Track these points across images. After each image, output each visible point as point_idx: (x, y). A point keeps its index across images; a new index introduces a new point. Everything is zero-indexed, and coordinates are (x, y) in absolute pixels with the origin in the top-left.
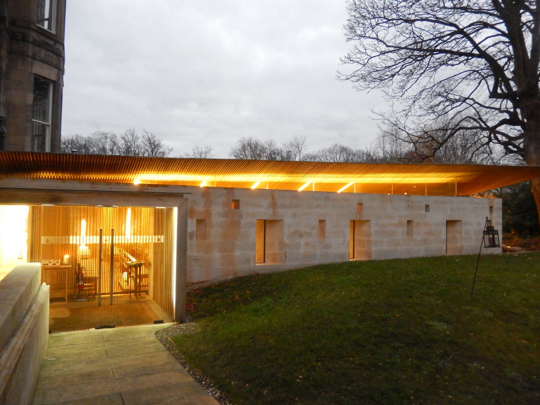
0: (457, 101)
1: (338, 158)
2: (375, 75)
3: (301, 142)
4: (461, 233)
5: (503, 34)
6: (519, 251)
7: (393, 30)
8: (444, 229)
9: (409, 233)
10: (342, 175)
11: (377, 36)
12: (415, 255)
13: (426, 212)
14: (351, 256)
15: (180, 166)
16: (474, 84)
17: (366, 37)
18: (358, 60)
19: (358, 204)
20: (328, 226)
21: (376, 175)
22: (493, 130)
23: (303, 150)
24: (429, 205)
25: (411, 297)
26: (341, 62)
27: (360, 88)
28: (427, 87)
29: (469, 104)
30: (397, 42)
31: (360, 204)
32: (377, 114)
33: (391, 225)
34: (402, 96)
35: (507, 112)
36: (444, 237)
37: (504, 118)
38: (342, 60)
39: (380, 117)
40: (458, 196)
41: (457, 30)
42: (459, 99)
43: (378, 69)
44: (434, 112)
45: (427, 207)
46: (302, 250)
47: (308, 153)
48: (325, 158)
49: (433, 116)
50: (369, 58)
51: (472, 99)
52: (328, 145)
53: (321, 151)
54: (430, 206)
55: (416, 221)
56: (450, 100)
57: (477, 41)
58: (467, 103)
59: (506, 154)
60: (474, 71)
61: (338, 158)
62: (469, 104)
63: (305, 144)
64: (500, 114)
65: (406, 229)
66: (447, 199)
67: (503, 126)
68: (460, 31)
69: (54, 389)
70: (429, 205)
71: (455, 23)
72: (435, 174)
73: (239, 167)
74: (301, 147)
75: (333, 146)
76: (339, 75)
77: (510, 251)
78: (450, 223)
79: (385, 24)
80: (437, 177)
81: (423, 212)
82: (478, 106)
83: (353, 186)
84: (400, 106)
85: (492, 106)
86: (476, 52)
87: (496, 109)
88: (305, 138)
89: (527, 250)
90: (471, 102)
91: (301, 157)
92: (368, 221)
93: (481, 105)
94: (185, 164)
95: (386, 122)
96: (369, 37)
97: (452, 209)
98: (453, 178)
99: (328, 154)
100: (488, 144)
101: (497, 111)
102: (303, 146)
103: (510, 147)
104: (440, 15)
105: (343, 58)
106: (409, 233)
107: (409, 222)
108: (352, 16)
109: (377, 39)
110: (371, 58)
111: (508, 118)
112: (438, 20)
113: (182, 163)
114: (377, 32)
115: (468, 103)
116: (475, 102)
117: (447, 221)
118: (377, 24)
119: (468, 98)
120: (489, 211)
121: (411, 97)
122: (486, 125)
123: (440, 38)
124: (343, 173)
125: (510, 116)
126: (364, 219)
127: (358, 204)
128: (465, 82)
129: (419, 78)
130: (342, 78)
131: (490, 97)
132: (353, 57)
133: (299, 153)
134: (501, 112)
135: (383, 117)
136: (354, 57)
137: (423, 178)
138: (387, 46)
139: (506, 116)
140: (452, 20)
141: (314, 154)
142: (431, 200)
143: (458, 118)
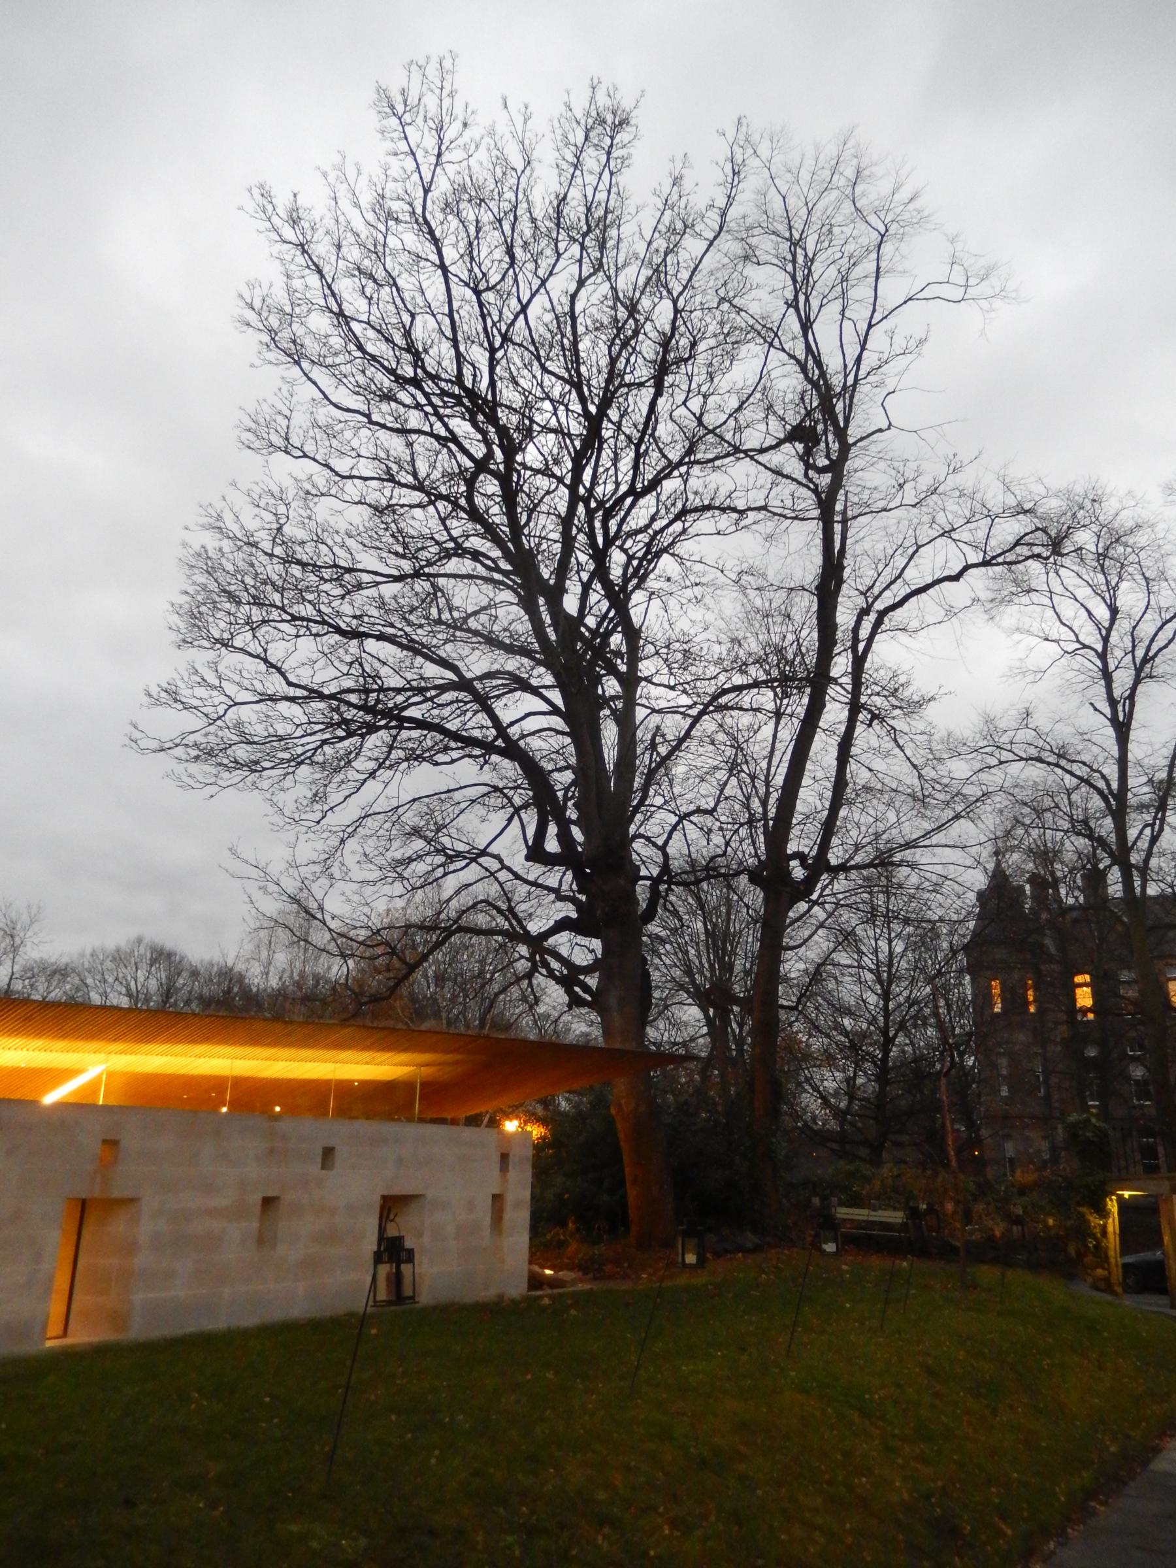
0: (459, 855)
1: (141, 979)
2: (242, 752)
3: (25, 918)
5: (555, 711)
6: (574, 1282)
7: (307, 646)
9: (264, 1240)
10: (61, 1044)
11: (265, 651)
12: (277, 1314)
13: (323, 1167)
14: (54, 1328)
16: (499, 818)
17: (236, 648)
18: (195, 702)
19: (105, 1142)
21: (180, 1048)
22: (537, 943)
23: (29, 944)
25: (129, 1503)
26: (146, 699)
27: (190, 781)
28: (376, 809)
29: (487, 869)
30: (318, 679)
31: (111, 1143)
32: (246, 862)
34: (318, 822)
37: (561, 915)
38: (150, 695)
39: (255, 873)
40: (422, 1120)
41: (455, 678)
42: (468, 852)
43: (256, 739)
44: (401, 877)
45: (328, 1153)
47: (45, 956)
48: (98, 977)
49: (398, 888)
51: (497, 857)
52: (116, 937)
53: (88, 951)
56: (442, 851)
57: (506, 717)
58: (480, 865)
59: (570, 1007)
60: (496, 789)
61: (141, 979)
62: (487, 869)
63: (36, 927)
64: (559, 904)
65: (255, 1225)
66: (389, 1129)
67: (564, 933)
68: (464, 684)
71: (456, 663)
72: (378, 1054)
74: (22, 934)
75: (128, 942)
76: (136, 735)
77: (552, 1283)
79: (284, 626)
80: (367, 1063)
81: (315, 1169)
82: (511, 876)
83: (97, 1080)
84: (310, 848)
86: (500, 743)
87: (550, 889)
88: (39, 908)
89: (595, 1278)
90: (494, 865)
91: (16, 968)
92: (132, 1201)
93: (517, 876)
95: (272, 887)
96: (243, 651)
97: (400, 1161)
98: (412, 1068)
99: (109, 964)
100: (529, 975)
101: (552, 896)
102: (29, 934)
104: (420, 635)
105: (154, 691)
106: (264, 1240)
108: (194, 583)
109: (266, 661)
110: (236, 704)
111: (574, 915)
112: (414, 648)
114: (267, 643)
115: (485, 865)
116: (504, 867)
118: (264, 622)
119: (483, 853)
120: (498, 1166)
121: (334, 829)
122: (524, 928)
123: (421, 691)
124: (64, 1036)
125: (578, 911)
126: (116, 1194)
127: (105, 1142)
128: (479, 810)
129: (365, 780)
130: (143, 744)
132: (185, 693)
133: (11, 956)
134: (560, 898)
135: (262, 874)
136: (187, 692)
137: (327, 1065)
138: (290, 684)
140: (448, 651)
141: (64, 960)
142: (338, 1131)
143: (465, 899)
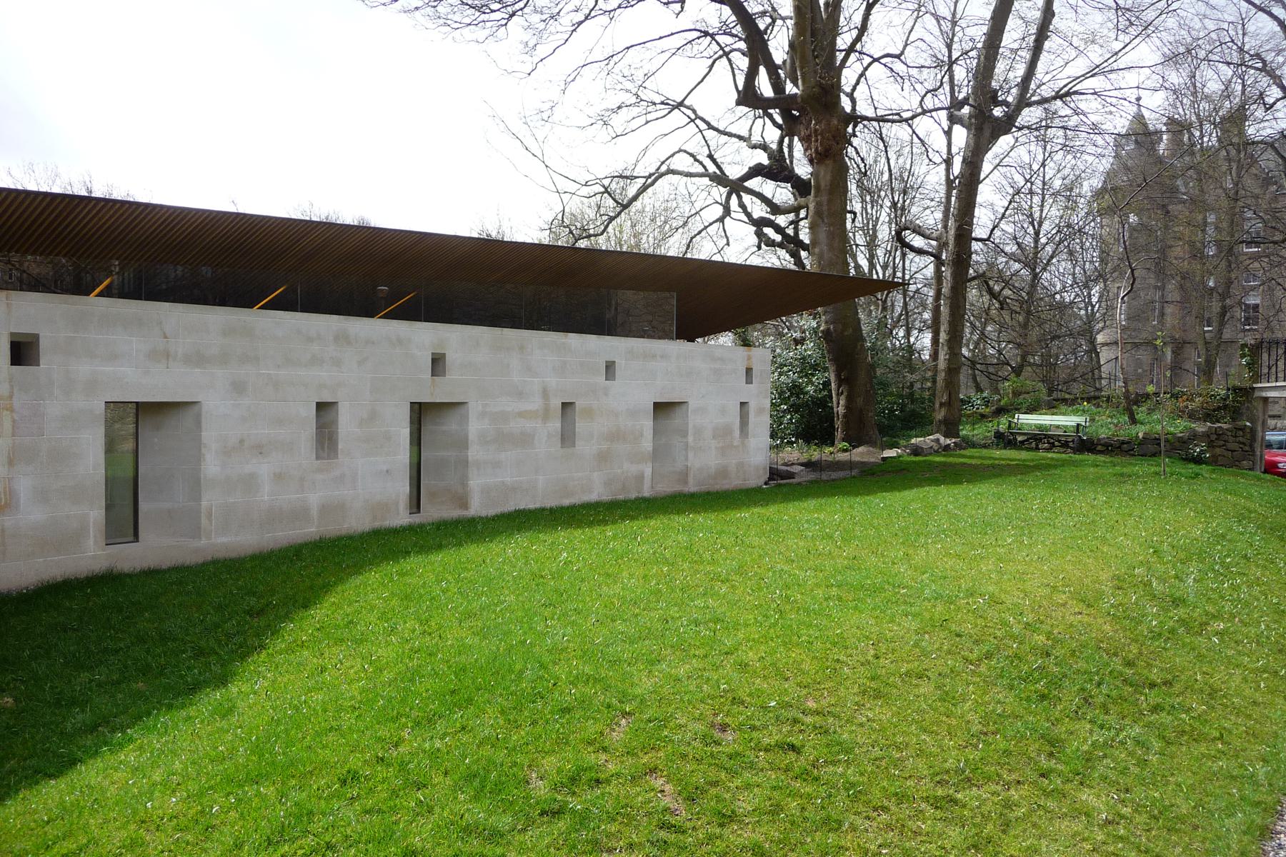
4: (684, 434)
8: (647, 423)
9: (567, 437)
15: (24, 211)
20: (346, 422)
22: (736, 187)
33: (521, 414)
35: (764, 147)
36: (647, 444)
45: (610, 368)
46: (266, 495)
55: (580, 404)
65: (558, 425)
69: (983, 416)
73: (239, 228)
78: (662, 409)
85: (730, 129)
87: (740, 138)
94: (28, 213)
103: (769, 231)
106: (567, 437)
107: (566, 406)
111: (766, 161)
117: (317, 403)
125: (770, 158)
131: (739, 103)
139: (762, 158)
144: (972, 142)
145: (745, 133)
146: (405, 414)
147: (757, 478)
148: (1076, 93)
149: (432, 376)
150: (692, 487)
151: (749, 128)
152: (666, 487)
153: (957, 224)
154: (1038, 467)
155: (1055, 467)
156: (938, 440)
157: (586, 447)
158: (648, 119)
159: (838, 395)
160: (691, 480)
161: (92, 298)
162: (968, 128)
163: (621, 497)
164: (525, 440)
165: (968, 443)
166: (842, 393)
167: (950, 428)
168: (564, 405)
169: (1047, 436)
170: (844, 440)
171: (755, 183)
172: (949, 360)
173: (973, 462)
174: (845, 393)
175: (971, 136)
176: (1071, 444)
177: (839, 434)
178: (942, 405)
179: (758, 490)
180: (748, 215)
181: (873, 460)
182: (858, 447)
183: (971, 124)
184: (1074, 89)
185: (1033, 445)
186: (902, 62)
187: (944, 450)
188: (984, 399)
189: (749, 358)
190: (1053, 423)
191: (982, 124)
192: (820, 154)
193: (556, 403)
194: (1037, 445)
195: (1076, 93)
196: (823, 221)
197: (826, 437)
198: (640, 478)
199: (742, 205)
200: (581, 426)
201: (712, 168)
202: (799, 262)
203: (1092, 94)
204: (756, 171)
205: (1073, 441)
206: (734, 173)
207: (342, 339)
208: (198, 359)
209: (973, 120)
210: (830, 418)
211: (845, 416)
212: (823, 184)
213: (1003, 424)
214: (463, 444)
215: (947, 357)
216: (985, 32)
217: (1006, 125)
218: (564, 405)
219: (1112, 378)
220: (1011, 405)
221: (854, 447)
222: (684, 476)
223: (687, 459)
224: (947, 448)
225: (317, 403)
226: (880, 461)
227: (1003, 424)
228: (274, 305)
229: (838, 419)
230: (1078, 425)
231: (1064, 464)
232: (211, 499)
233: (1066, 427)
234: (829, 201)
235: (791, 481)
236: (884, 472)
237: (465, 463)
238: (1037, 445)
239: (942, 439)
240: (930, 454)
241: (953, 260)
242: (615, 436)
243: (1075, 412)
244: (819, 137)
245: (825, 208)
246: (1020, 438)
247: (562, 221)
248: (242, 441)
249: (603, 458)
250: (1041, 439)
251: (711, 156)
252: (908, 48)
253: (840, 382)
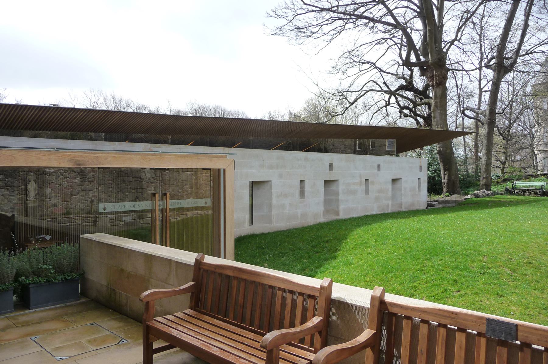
8: (390, 186)
9: (367, 192)
24: (380, 165)
36: (390, 194)
50: (296, 15)
54: (334, 165)
55: (370, 180)
65: (364, 187)
69: (498, 182)
70: (380, 165)
78: (394, 181)
81: (376, 171)
106: (367, 192)
110: (298, 15)
111: (405, 84)
113: (94, 120)
117: (324, 180)
132: (280, 12)
139: (403, 82)
144: (496, 76)
145: (395, 73)
146: (322, 183)
147: (423, 206)
148: (535, 52)
149: (330, 171)
150: (403, 209)
151: (396, 70)
152: (396, 209)
153: (490, 108)
154: (535, 201)
155: (538, 201)
156: (484, 192)
157: (372, 195)
158: (361, 69)
159: (444, 175)
160: (403, 206)
161: (232, 148)
162: (494, 70)
163: (382, 212)
164: (354, 192)
165: (494, 193)
166: (446, 174)
167: (487, 187)
168: (366, 180)
169: (528, 190)
170: (447, 192)
171: (402, 92)
172: (487, 161)
173: (503, 200)
174: (447, 174)
175: (496, 74)
176: (538, 193)
177: (444, 190)
178: (483, 178)
179: (423, 210)
180: (399, 105)
181: (460, 200)
182: (453, 195)
183: (496, 69)
184: (535, 50)
185: (522, 193)
186: (461, 43)
187: (487, 196)
188: (496, 175)
189: (421, 162)
190: (530, 185)
191: (500, 69)
192: (438, 84)
193: (363, 180)
194: (524, 194)
195: (535, 52)
196: (438, 109)
197: (439, 192)
198: (388, 206)
199: (397, 102)
200: (370, 187)
201: (385, 89)
202: (418, 123)
203: (541, 52)
204: (402, 88)
205: (540, 192)
206: (393, 89)
207: (306, 159)
208: (271, 167)
209: (497, 68)
210: (440, 183)
211: (447, 183)
212: (438, 95)
213: (509, 185)
214: (338, 194)
215: (486, 159)
216: (501, 33)
217: (510, 68)
218: (366, 180)
219: (466, 160)
220: (510, 178)
221: (451, 195)
222: (401, 205)
223: (402, 199)
224: (488, 195)
225: (324, 180)
226: (463, 200)
227: (509, 185)
228: (239, 147)
229: (444, 184)
230: (542, 185)
231: (542, 200)
232: (274, 212)
233: (536, 186)
234: (441, 101)
235: (434, 207)
236: (468, 204)
237: (338, 200)
238: (524, 194)
239: (486, 191)
240: (482, 197)
241: (488, 122)
242: (380, 191)
243: (539, 180)
244: (437, 78)
245: (439, 104)
246: (516, 191)
247: (314, 109)
248: (281, 193)
249: (377, 199)
250: (525, 191)
251: (385, 83)
252: (462, 36)
253: (445, 170)
